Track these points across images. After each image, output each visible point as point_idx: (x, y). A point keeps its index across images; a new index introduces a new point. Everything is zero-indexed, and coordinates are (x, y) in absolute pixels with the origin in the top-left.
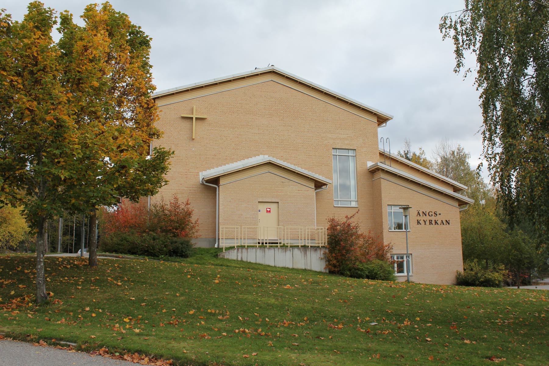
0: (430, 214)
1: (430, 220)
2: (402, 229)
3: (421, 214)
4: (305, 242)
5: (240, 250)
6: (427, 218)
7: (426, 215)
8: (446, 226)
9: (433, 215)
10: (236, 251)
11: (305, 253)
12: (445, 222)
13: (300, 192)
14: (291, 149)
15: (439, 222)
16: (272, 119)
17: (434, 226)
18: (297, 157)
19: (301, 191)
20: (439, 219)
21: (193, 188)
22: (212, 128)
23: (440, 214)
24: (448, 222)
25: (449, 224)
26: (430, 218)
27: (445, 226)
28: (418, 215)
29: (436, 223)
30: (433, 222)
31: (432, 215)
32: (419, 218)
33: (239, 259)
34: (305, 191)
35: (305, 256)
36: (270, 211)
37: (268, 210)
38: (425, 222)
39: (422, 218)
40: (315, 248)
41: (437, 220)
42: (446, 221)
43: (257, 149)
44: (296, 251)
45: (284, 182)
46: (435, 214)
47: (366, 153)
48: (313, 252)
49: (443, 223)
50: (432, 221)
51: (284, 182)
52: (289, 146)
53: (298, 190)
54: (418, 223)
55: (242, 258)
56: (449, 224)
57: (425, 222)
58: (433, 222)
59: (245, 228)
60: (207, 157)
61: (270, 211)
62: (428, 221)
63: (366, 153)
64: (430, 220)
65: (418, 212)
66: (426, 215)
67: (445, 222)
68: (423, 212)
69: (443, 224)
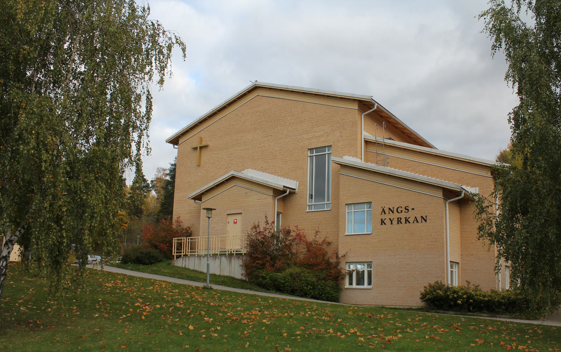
0: (399, 210)
1: (398, 218)
2: (182, 242)
3: (387, 211)
4: (215, 252)
5: (184, 258)
6: (396, 216)
7: (393, 212)
8: (421, 225)
9: (404, 210)
10: (182, 259)
11: (230, 261)
12: (419, 219)
13: (260, 200)
14: (270, 158)
15: (411, 220)
16: (257, 133)
17: (404, 225)
18: (274, 166)
19: (261, 199)
20: (411, 215)
21: (197, 207)
22: (213, 153)
23: (413, 209)
24: (424, 219)
25: (426, 221)
26: (399, 215)
27: (419, 225)
28: (383, 213)
29: (407, 220)
30: (403, 221)
31: (402, 211)
32: (383, 216)
33: (184, 266)
34: (264, 199)
35: (230, 264)
36: (236, 222)
37: (235, 221)
38: (392, 221)
39: (387, 217)
40: (239, 255)
41: (408, 217)
42: (422, 217)
43: (242, 165)
44: (223, 259)
45: (248, 193)
46: (406, 209)
47: (343, 146)
48: (236, 260)
49: (417, 220)
50: (401, 218)
51: (248, 193)
52: (268, 156)
53: (259, 199)
54: (383, 222)
55: (185, 266)
56: (426, 221)
57: (392, 221)
58: (403, 221)
59: (189, 239)
60: (208, 179)
61: (236, 222)
62: (397, 220)
63: (343, 146)
64: (398, 218)
65: (383, 209)
66: (393, 212)
67: (419, 219)
68: (390, 209)
69: (417, 222)
